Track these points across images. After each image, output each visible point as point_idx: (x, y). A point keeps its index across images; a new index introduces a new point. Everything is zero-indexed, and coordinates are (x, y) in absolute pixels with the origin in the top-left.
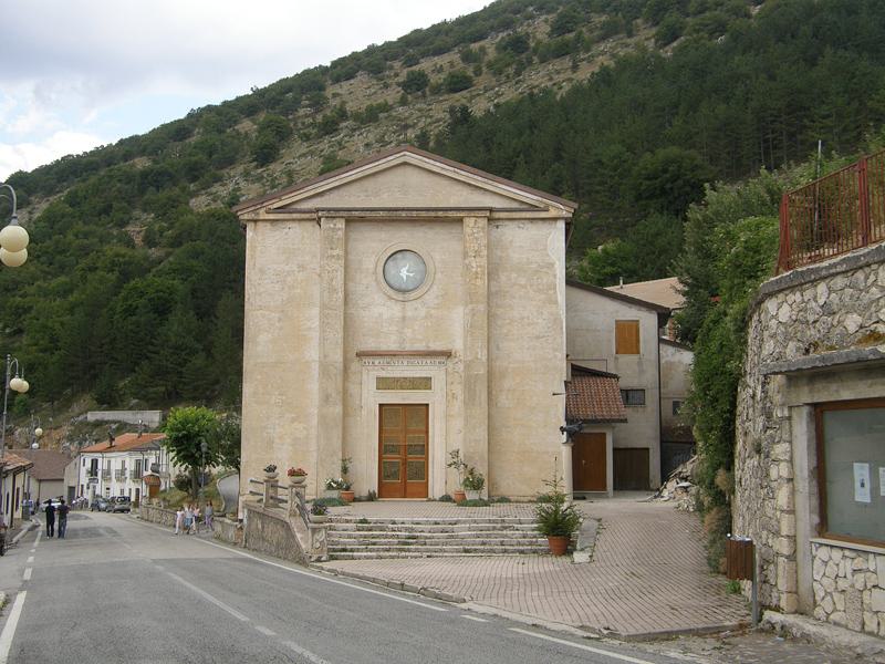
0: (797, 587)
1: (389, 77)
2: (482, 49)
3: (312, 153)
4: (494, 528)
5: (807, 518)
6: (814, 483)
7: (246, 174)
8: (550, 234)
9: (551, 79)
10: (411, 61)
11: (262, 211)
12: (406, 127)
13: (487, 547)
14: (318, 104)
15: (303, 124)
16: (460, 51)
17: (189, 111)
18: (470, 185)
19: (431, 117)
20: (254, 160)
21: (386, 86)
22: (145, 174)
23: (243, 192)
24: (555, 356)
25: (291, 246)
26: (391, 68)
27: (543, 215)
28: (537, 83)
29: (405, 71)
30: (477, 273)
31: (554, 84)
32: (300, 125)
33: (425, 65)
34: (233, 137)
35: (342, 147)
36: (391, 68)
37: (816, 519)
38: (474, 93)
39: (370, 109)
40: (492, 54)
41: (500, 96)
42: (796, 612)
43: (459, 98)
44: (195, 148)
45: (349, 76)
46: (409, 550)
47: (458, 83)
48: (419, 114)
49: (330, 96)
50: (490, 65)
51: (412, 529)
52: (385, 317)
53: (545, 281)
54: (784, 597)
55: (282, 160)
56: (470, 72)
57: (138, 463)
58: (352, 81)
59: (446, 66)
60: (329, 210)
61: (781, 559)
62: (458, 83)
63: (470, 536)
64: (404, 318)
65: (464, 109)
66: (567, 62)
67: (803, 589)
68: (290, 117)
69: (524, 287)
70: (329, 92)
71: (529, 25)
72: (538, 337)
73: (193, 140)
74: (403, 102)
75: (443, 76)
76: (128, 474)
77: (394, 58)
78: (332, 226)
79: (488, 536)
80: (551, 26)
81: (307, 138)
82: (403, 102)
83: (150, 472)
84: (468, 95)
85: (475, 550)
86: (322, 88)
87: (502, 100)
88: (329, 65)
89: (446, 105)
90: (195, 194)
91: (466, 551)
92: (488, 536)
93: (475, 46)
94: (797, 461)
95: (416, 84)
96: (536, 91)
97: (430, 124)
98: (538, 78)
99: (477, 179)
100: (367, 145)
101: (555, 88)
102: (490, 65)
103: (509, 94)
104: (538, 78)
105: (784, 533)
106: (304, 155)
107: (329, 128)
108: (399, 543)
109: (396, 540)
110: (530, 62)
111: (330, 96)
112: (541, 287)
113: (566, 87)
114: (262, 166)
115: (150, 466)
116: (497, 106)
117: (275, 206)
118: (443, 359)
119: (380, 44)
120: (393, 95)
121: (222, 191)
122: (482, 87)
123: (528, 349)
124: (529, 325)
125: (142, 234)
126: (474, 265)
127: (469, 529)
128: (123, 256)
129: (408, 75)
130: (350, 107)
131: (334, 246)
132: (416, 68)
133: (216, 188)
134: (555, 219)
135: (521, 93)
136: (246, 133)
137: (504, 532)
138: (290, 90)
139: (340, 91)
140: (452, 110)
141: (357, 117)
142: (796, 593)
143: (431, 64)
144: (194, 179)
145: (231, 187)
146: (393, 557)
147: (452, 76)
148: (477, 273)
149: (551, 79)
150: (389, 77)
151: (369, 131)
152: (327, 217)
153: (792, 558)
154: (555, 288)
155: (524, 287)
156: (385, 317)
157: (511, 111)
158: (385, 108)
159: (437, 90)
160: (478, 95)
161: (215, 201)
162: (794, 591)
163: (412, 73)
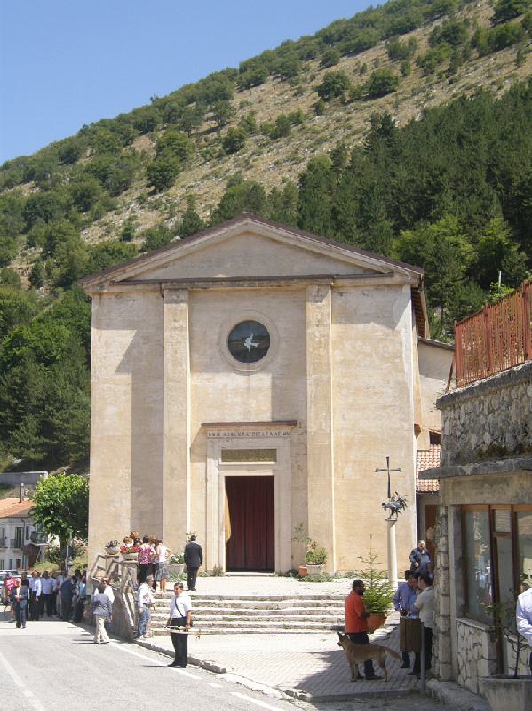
0: (451, 659)
1: (305, 80)
2: (412, 43)
3: (216, 175)
4: (318, 605)
5: (455, 601)
6: (460, 570)
7: (141, 200)
8: (396, 299)
9: (490, 77)
10: (328, 62)
11: (107, 284)
12: (320, 141)
13: (309, 623)
14: (222, 118)
15: (206, 140)
16: (387, 46)
17: (81, 127)
18: (314, 253)
19: (350, 128)
20: (152, 184)
21: (300, 92)
22: (31, 204)
23: (139, 221)
24: (403, 427)
25: (136, 319)
26: (306, 69)
27: (388, 281)
28: (473, 82)
29: (323, 73)
30: (320, 342)
31: (493, 83)
32: (203, 142)
33: (346, 65)
34: (128, 157)
35: (248, 166)
36: (306, 69)
37: (461, 601)
38: (401, 97)
39: (280, 121)
40: (423, 48)
41: (430, 99)
42: (449, 680)
43: (382, 104)
44: (86, 171)
45: (258, 82)
46: (232, 627)
47: (380, 88)
48: (338, 125)
49: (237, 107)
50: (420, 63)
51: (239, 606)
52: (230, 387)
53: (391, 348)
54: (441, 666)
55: (182, 183)
56: (396, 72)
57: (19, 530)
58: (262, 87)
59: (370, 65)
60: (172, 281)
61: (440, 635)
62: (380, 88)
63: (266, 614)
64: (248, 388)
65: (386, 120)
66: (508, 55)
67: (454, 661)
68: (193, 132)
69: (370, 355)
70: (237, 99)
71: (469, 9)
72: (385, 407)
73: (84, 162)
74: (318, 110)
75: (366, 77)
76: (8, 543)
77: (310, 57)
78: (175, 297)
79: (311, 613)
80: (495, 9)
81: (207, 157)
82: (318, 110)
83: (29, 542)
84: (394, 99)
85: (295, 627)
86: (226, 97)
87: (434, 103)
88: (238, 67)
89: (366, 114)
90: (85, 225)
91: (285, 627)
92: (311, 613)
93: (404, 39)
94: (450, 553)
95: (330, 90)
96: (468, 94)
97: (348, 137)
98: (476, 75)
99: (320, 246)
100: (277, 163)
101: (495, 88)
102: (420, 63)
103: (441, 96)
104: (476, 75)
105: (441, 613)
106: (206, 177)
107: (232, 145)
108: (225, 619)
109: (221, 616)
110: (466, 56)
111: (237, 107)
112: (387, 355)
113: (508, 85)
114: (161, 190)
115: (30, 534)
116: (425, 112)
117: (119, 278)
118: (287, 429)
119: (295, 40)
120: (305, 104)
121: (118, 220)
122: (409, 89)
123: (374, 419)
124: (375, 394)
125: (30, 271)
126: (317, 334)
127: (295, 605)
128: (8, 298)
129: (325, 79)
130: (260, 119)
131: (177, 319)
132: (334, 69)
133: (109, 217)
134: (401, 285)
135: (454, 96)
136: (144, 152)
137: (328, 608)
138: (191, 100)
139: (249, 99)
140: (373, 120)
141: (264, 130)
142: (451, 663)
143: (354, 62)
144: (87, 208)
145: (126, 215)
146: (212, 633)
147: (374, 78)
148: (320, 342)
149: (490, 77)
150: (305, 80)
151: (280, 147)
152: (170, 289)
153: (447, 633)
154: (401, 356)
155: (370, 355)
156: (230, 387)
157: (435, 122)
158: (297, 119)
159: (356, 97)
160: (404, 99)
161: (108, 232)
162: (449, 662)
163: (329, 75)
